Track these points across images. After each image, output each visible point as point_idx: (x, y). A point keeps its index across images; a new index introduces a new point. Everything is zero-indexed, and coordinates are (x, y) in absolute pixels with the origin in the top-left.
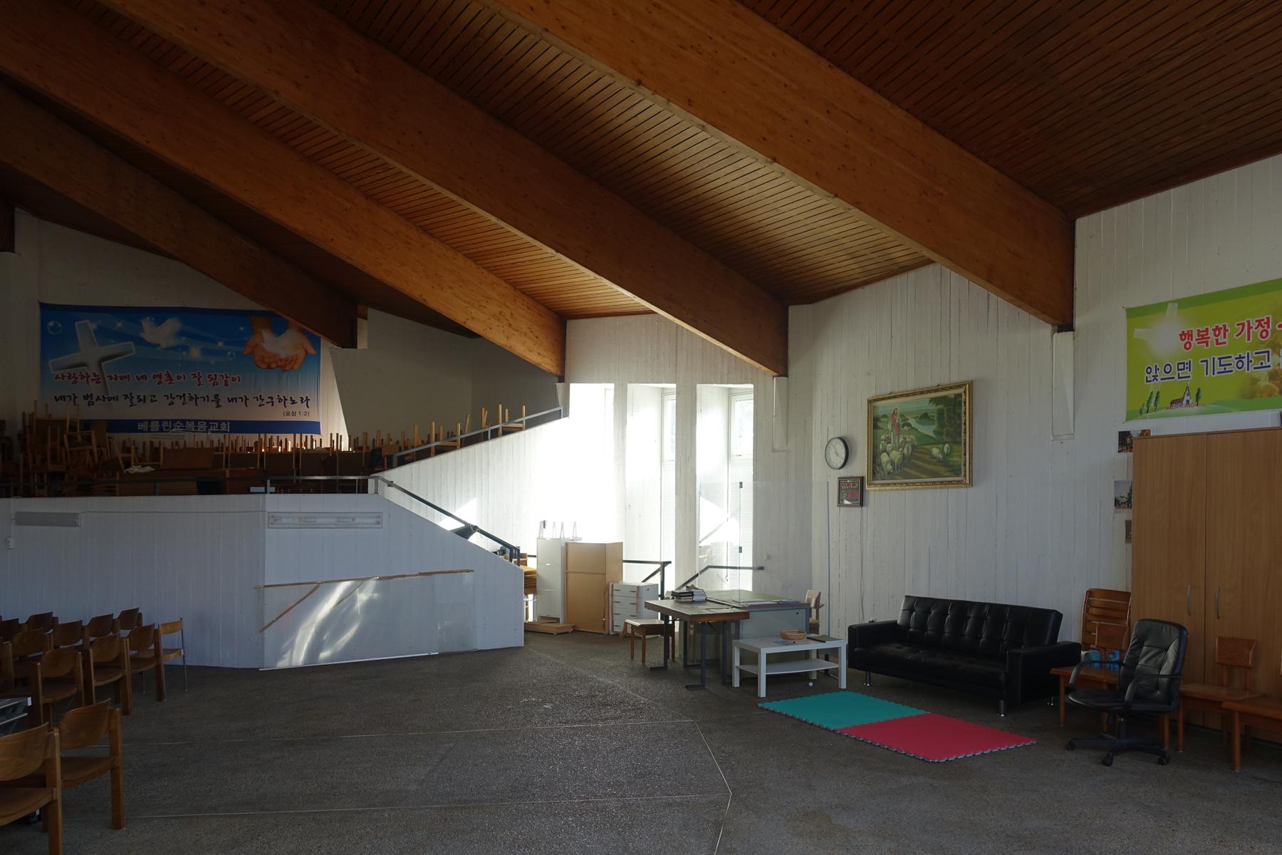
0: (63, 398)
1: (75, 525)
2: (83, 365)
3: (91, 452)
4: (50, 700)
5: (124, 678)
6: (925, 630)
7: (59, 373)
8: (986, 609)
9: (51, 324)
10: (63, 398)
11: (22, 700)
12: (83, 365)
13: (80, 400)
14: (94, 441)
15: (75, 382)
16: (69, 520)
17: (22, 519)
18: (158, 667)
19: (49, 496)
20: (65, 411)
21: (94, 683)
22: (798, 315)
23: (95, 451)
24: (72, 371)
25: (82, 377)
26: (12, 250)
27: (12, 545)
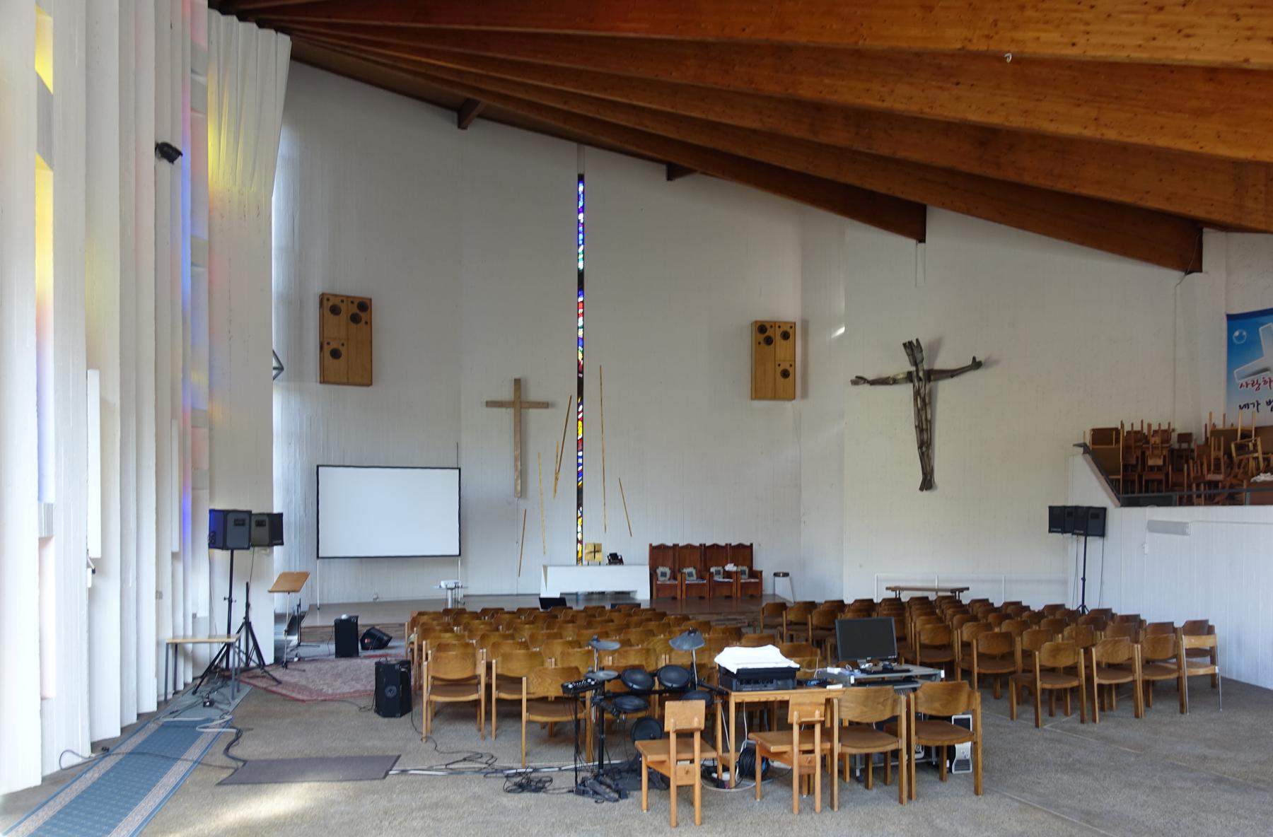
0: (1247, 406)
1: (1184, 533)
2: (1265, 370)
3: (1257, 459)
4: (1048, 686)
5: (1134, 682)
6: (622, 600)
7: (1243, 381)
8: (231, 519)
9: (1237, 334)
10: (1247, 406)
11: (936, 671)
12: (1265, 370)
13: (1263, 406)
14: (1259, 448)
15: (1258, 389)
16: (1180, 529)
17: (1153, 527)
18: (1179, 679)
19: (1206, 504)
20: (1243, 420)
21: (1096, 681)
22: (455, 115)
23: (1261, 459)
24: (1255, 378)
25: (1265, 382)
26: (1200, 271)
27: (1147, 551)
